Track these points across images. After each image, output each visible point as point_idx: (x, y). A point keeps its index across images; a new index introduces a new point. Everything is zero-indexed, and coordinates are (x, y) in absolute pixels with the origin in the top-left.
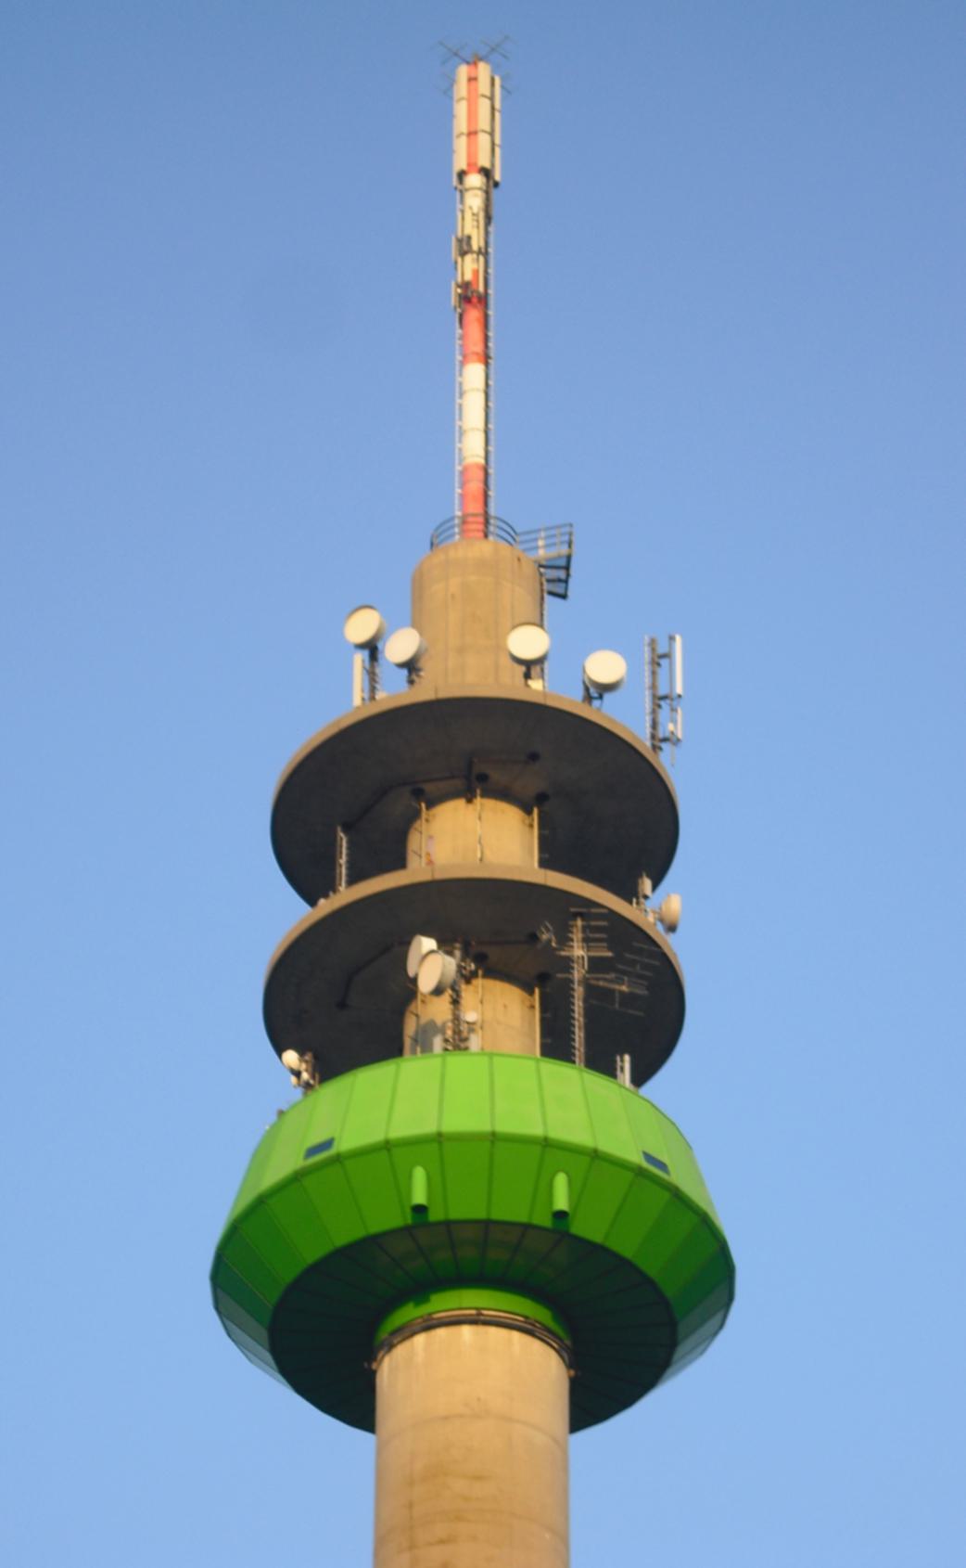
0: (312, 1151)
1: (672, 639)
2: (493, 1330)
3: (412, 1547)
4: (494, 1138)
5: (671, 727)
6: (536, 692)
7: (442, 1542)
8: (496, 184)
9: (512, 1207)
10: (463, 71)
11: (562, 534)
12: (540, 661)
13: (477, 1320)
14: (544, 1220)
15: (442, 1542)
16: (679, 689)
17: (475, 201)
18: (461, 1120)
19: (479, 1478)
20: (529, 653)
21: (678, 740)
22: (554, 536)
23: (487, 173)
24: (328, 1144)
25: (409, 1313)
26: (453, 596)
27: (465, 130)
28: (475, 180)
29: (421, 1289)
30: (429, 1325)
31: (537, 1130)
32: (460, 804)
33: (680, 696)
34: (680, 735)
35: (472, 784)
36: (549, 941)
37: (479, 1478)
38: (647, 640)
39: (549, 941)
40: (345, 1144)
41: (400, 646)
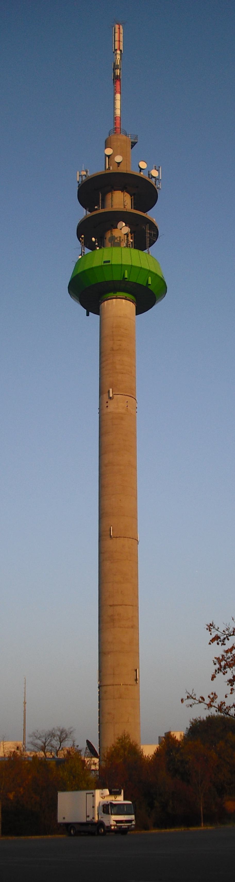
0: (105, 262)
1: (159, 167)
2: (128, 301)
3: (113, 340)
4: (141, 268)
5: (159, 186)
6: (142, 175)
7: (119, 340)
8: (122, 54)
9: (141, 281)
10: (117, 26)
11: (134, 137)
12: (143, 169)
13: (126, 299)
14: (145, 284)
15: (119, 340)
16: (161, 178)
17: (118, 57)
18: (136, 263)
19: (126, 330)
20: (142, 167)
21: (160, 189)
22: (132, 137)
23: (121, 51)
24: (109, 262)
25: (111, 295)
26: (119, 146)
27: (117, 40)
28: (118, 52)
29: (115, 290)
30: (116, 298)
31: (148, 268)
32: (120, 192)
33: (161, 180)
34: (161, 188)
35: (123, 189)
36: (144, 228)
37: (126, 330)
38: (154, 166)
39: (144, 228)
40: (113, 262)
41: (118, 159)
